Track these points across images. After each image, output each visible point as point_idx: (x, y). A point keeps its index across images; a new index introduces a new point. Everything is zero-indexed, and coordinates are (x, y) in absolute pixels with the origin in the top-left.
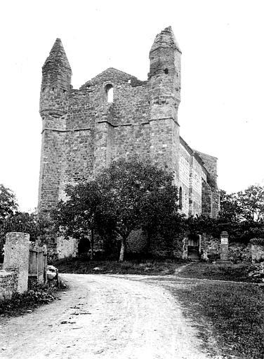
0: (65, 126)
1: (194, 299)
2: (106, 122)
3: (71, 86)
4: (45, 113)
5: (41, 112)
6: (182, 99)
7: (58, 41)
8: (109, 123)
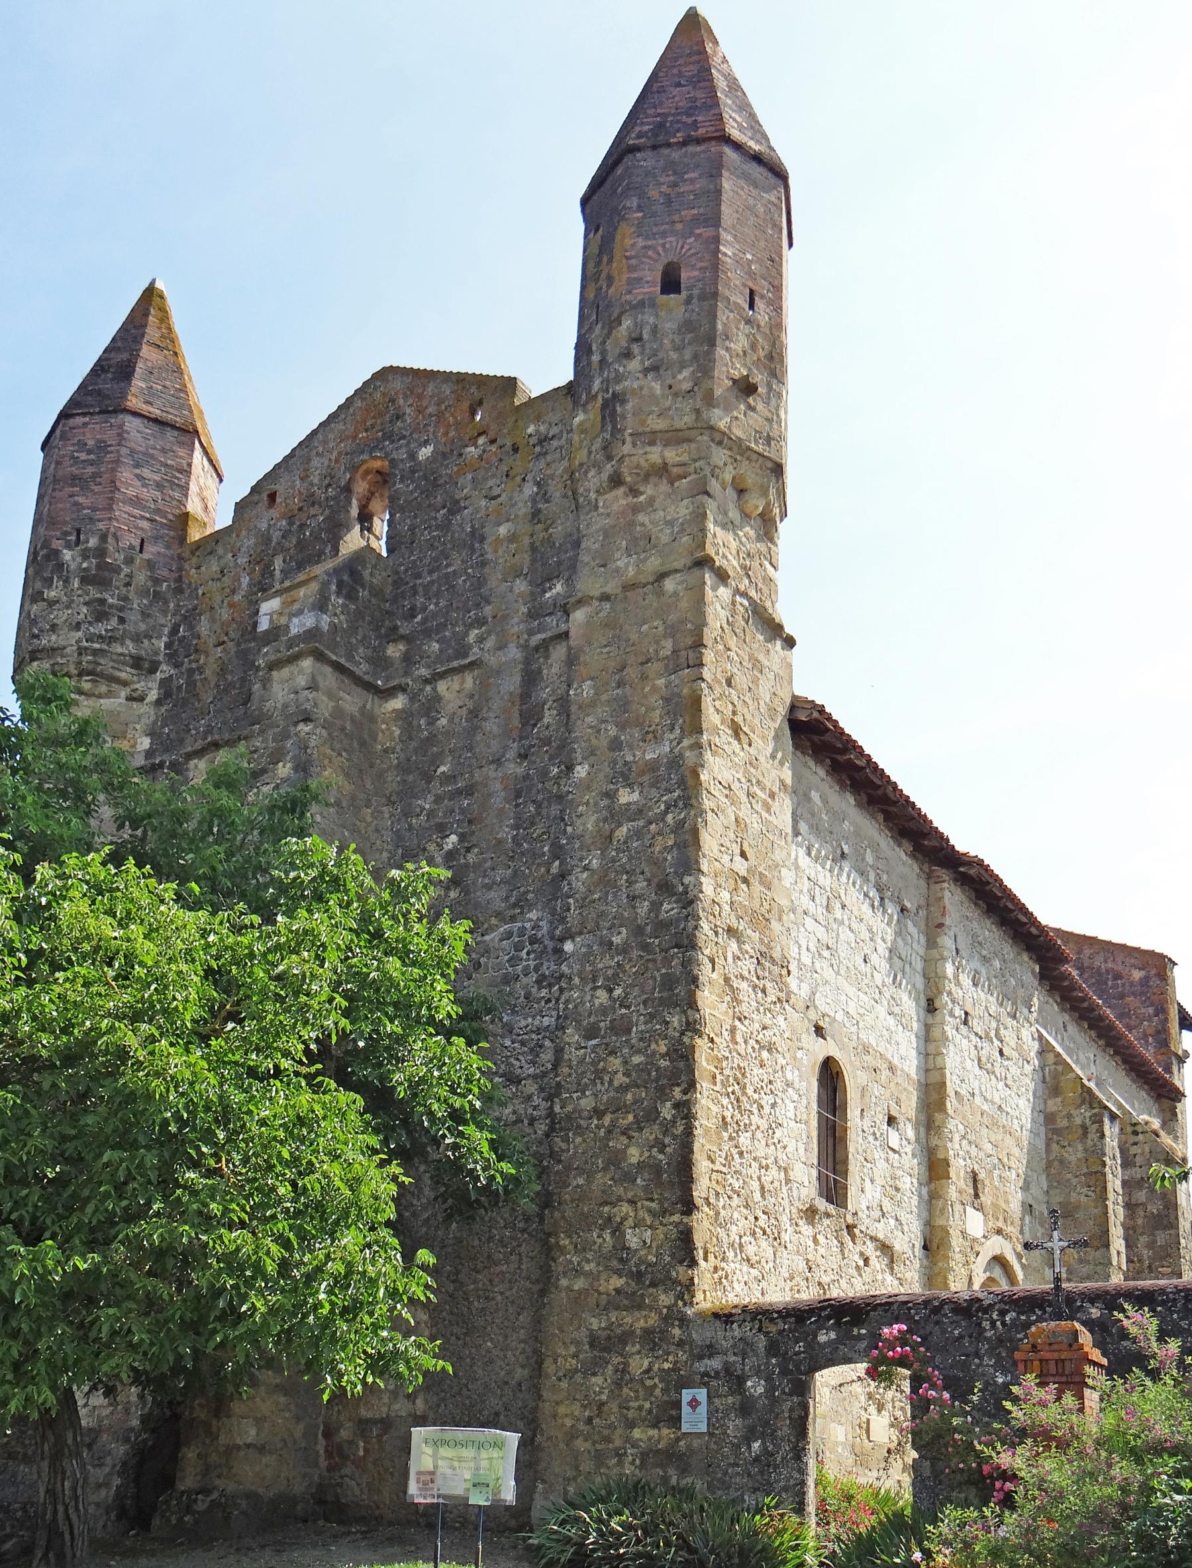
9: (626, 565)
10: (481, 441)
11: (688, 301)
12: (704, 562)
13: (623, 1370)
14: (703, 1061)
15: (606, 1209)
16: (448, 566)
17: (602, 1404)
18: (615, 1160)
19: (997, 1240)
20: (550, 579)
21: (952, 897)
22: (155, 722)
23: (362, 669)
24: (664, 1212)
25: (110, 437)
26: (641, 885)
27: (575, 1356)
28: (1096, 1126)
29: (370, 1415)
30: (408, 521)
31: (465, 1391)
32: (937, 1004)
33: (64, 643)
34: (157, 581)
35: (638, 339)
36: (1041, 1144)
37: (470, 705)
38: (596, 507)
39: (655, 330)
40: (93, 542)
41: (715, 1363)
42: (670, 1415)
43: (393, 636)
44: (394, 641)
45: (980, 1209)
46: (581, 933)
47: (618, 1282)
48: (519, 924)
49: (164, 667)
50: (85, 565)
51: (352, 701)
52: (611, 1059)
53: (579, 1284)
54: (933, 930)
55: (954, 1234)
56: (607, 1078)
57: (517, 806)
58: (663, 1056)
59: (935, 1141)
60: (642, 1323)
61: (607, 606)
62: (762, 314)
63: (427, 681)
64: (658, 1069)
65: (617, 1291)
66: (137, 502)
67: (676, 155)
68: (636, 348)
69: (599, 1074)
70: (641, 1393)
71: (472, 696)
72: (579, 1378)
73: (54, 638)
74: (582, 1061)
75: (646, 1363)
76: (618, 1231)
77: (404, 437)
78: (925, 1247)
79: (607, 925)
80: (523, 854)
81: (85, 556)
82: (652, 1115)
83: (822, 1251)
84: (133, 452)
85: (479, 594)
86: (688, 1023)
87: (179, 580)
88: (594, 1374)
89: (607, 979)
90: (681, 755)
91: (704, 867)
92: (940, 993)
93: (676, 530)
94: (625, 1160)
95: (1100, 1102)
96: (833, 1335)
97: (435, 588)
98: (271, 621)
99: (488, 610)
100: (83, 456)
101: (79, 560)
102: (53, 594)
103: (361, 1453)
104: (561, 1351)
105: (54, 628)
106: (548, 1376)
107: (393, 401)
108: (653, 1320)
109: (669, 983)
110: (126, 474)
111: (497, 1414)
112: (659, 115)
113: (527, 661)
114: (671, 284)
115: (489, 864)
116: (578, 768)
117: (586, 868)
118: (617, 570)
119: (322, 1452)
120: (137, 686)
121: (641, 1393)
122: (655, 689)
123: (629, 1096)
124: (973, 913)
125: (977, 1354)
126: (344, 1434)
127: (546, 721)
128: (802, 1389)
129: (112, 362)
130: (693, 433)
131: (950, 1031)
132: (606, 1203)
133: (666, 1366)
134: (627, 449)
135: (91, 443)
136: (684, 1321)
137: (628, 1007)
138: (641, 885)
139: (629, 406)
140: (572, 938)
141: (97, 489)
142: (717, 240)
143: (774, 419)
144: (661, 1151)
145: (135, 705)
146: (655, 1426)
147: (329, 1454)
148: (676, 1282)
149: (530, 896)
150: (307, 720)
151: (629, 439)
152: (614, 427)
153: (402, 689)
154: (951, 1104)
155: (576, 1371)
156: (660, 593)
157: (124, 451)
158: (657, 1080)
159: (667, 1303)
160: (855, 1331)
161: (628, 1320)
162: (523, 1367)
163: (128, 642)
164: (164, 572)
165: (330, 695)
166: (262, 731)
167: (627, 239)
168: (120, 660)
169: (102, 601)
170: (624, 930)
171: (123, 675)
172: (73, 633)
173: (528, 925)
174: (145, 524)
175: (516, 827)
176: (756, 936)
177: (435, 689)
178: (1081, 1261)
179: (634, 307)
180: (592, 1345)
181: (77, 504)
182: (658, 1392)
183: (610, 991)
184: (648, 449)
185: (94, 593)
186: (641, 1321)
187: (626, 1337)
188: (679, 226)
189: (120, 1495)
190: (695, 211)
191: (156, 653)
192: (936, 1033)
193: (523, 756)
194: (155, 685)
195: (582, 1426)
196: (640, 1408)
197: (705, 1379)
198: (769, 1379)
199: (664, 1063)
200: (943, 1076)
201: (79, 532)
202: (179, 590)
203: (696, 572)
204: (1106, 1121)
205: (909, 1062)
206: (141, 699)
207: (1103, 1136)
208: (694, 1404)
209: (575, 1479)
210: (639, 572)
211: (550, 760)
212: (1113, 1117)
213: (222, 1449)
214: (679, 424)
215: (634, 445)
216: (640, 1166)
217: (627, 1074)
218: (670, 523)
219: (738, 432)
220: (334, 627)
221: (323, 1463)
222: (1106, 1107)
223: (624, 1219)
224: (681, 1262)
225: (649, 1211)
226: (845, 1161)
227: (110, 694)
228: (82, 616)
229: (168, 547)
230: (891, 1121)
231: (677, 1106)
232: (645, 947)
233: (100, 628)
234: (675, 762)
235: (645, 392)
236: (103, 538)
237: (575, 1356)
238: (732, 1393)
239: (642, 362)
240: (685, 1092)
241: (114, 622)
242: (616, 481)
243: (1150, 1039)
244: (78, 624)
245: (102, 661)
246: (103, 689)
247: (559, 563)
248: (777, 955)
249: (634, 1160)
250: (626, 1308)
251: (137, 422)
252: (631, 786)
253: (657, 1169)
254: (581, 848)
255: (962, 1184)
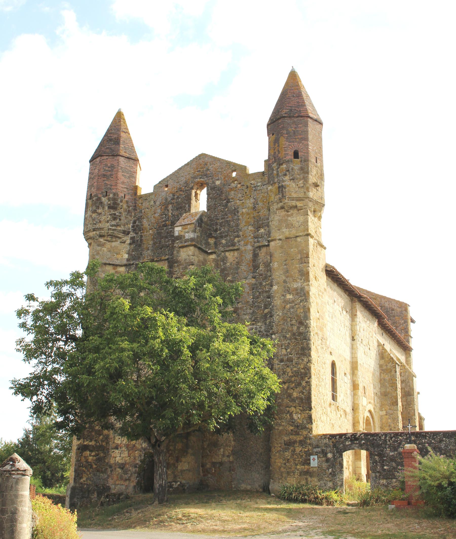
0: (126, 256)
1: (116, 371)
2: (195, 246)
3: (136, 188)
4: (91, 234)
5: (85, 233)
6: (327, 200)
7: (293, 76)
8: (199, 249)
9: (286, 232)
10: (236, 182)
11: (301, 161)
12: (308, 235)
13: (294, 450)
14: (313, 371)
15: (288, 408)
16: (227, 218)
17: (288, 459)
18: (290, 395)
19: (370, 405)
20: (260, 228)
21: (358, 306)
22: (129, 250)
23: (203, 247)
24: (304, 410)
25: (115, 163)
26: (294, 322)
27: (280, 447)
28: (394, 369)
29: (216, 461)
30: (213, 202)
31: (245, 455)
32: (355, 338)
33: (104, 226)
34: (129, 207)
35: (288, 171)
36: (378, 374)
37: (237, 260)
38: (276, 213)
39: (292, 169)
40: (111, 196)
41: (319, 449)
42: (307, 462)
43: (210, 236)
44: (211, 237)
45: (366, 397)
46: (277, 333)
47: (292, 428)
48: (255, 326)
49: (131, 233)
50: (109, 203)
51: (202, 257)
52: (287, 368)
53: (281, 428)
54: (353, 316)
55: (360, 405)
56: (286, 374)
57: (253, 292)
58: (302, 369)
59: (355, 379)
60: (299, 439)
61: (281, 242)
62: (319, 165)
63: (223, 252)
64: (301, 372)
65: (292, 430)
66: (123, 183)
67: (295, 119)
68: (287, 173)
69: (284, 373)
70: (299, 457)
71: (237, 258)
72: (282, 453)
73: (100, 225)
74: (279, 368)
75: (300, 449)
76: (291, 414)
77: (211, 176)
78: (353, 410)
79: (285, 331)
80: (255, 306)
81: (109, 199)
82: (299, 384)
83: (332, 415)
84: (122, 168)
85: (237, 229)
86: (309, 360)
87: (135, 206)
88: (286, 452)
89: (285, 346)
90: (304, 287)
91: (311, 318)
92: (355, 335)
93: (300, 224)
94: (292, 395)
95: (395, 362)
96: (350, 443)
97: (224, 224)
98: (179, 233)
99: (241, 233)
100: (107, 169)
101: (107, 201)
102: (99, 211)
103: (213, 471)
104: (276, 445)
105: (100, 222)
106: (273, 452)
107: (206, 164)
108: (302, 438)
109: (303, 349)
110: (120, 174)
111: (255, 461)
112: (290, 106)
113: (254, 251)
114: (296, 155)
115: (245, 308)
116: (274, 287)
117: (278, 315)
118: (283, 232)
119: (201, 471)
120: (123, 239)
121: (299, 457)
122: (296, 268)
123: (293, 379)
124: (362, 309)
125: (385, 448)
126: (208, 466)
127: (261, 268)
128: (341, 456)
129: (112, 137)
130: (304, 199)
131: (358, 345)
132: (288, 407)
133: (306, 450)
134: (286, 201)
135: (109, 165)
136: (310, 438)
137: (292, 355)
138: (294, 322)
139: (287, 190)
140: (275, 334)
141: (112, 179)
142: (308, 145)
143: (322, 193)
144: (303, 394)
145: (122, 244)
146: (303, 465)
147: (203, 472)
148: (308, 428)
149: (258, 319)
150: (193, 265)
151: (287, 199)
152: (283, 194)
153: (214, 253)
154: (359, 367)
155: (281, 451)
156: (296, 241)
157: (119, 168)
158: (301, 375)
159: (306, 434)
160: (355, 442)
161: (295, 438)
162: (262, 449)
163: (122, 226)
164: (131, 204)
165: (198, 257)
166: (178, 266)
167: (283, 141)
168: (119, 231)
169: (115, 214)
170: (290, 333)
171: (120, 236)
172: (106, 224)
173: (258, 327)
174: (125, 190)
175: (253, 298)
176: (321, 333)
177: (225, 254)
178: (390, 409)
179: (287, 162)
180: (285, 444)
181: (105, 183)
182: (304, 456)
183: (286, 350)
184: (292, 201)
185: (112, 212)
186: (298, 438)
187: (295, 442)
188: (298, 140)
189: (138, 483)
190: (302, 136)
191: (129, 229)
192: (355, 347)
193: (254, 277)
194: (129, 238)
195: (283, 465)
196: (299, 461)
197: (316, 453)
198: (333, 453)
199: (303, 371)
200: (357, 359)
201: (107, 192)
202: (135, 210)
203: (306, 237)
204: (397, 366)
205: (347, 355)
206: (124, 242)
207: (396, 372)
208: (314, 459)
209: (281, 479)
210: (290, 234)
211: (263, 280)
212: (398, 365)
213: (179, 471)
214: (300, 196)
215: (288, 200)
216: (297, 398)
217: (292, 373)
218: (298, 222)
219: (315, 198)
220: (198, 236)
221: (202, 474)
222: (397, 363)
223: (292, 412)
224: (309, 423)
225: (300, 409)
226: (336, 389)
227: (116, 241)
228: (109, 219)
229: (131, 196)
230: (345, 374)
231: (307, 382)
232: (296, 339)
233: (114, 223)
234: (302, 289)
235: (290, 186)
236: (114, 194)
237: (280, 447)
238: (323, 457)
239: (289, 177)
240: (309, 379)
241: (118, 220)
242: (282, 208)
243: (403, 331)
244: (108, 221)
245: (115, 232)
246: (114, 240)
247: (263, 223)
248: (325, 337)
249: (295, 396)
250: (294, 435)
251: (122, 158)
252: (290, 293)
253: (301, 399)
254: (276, 309)
255: (362, 390)
